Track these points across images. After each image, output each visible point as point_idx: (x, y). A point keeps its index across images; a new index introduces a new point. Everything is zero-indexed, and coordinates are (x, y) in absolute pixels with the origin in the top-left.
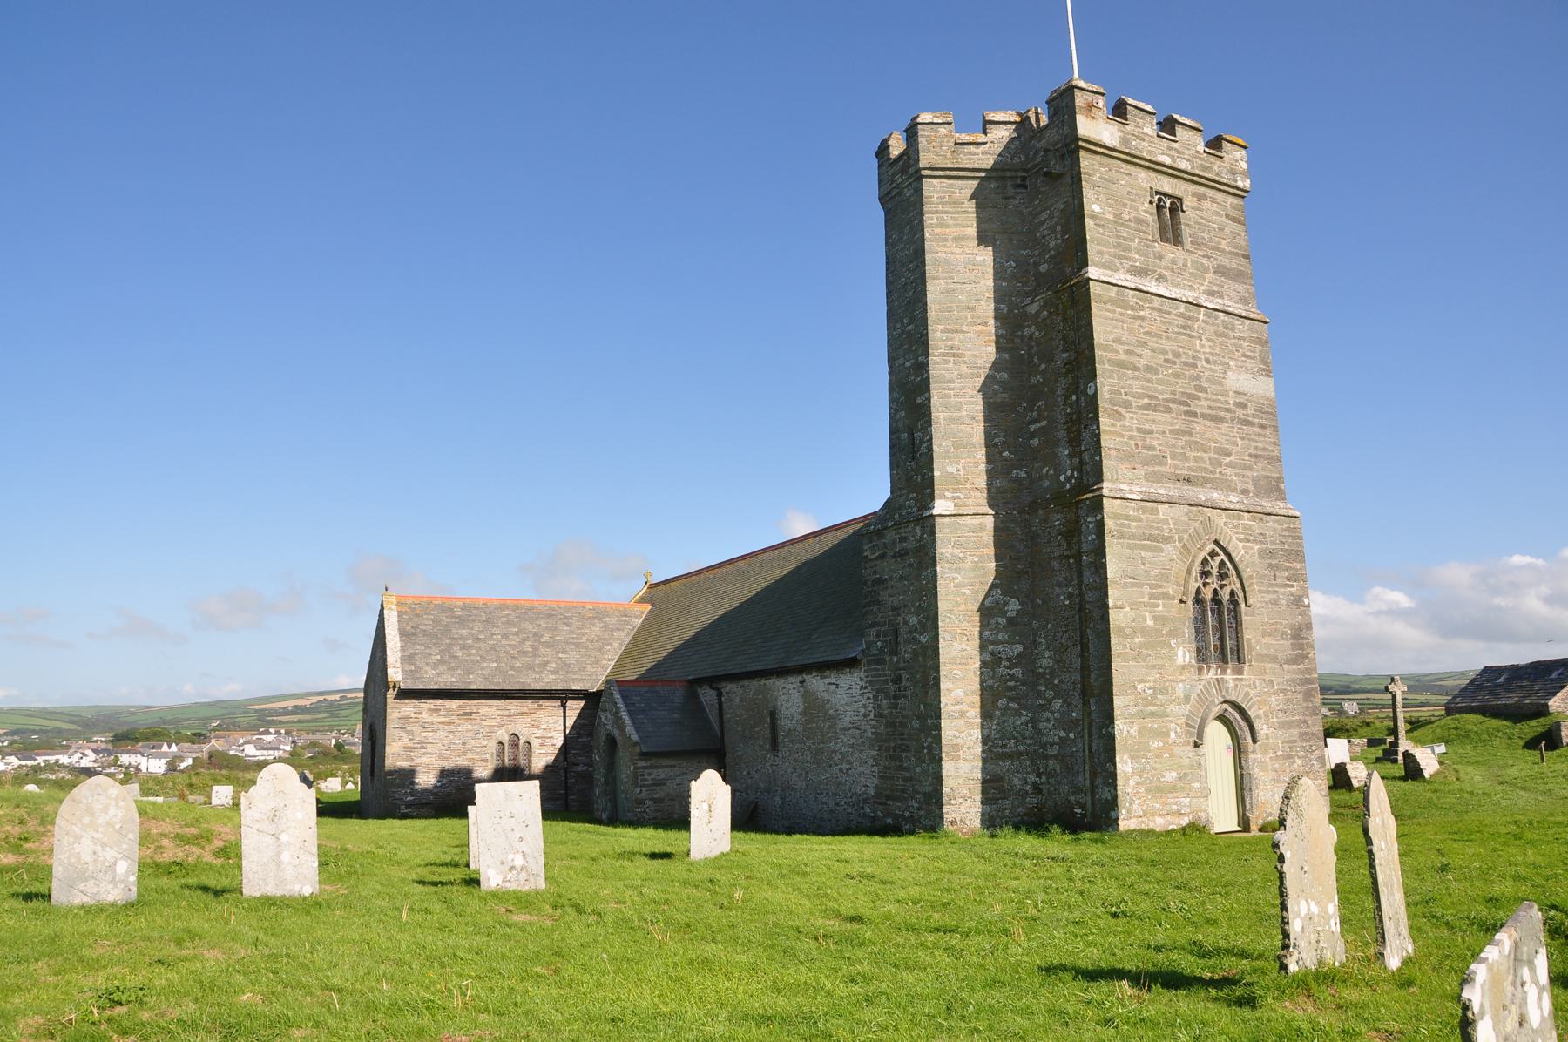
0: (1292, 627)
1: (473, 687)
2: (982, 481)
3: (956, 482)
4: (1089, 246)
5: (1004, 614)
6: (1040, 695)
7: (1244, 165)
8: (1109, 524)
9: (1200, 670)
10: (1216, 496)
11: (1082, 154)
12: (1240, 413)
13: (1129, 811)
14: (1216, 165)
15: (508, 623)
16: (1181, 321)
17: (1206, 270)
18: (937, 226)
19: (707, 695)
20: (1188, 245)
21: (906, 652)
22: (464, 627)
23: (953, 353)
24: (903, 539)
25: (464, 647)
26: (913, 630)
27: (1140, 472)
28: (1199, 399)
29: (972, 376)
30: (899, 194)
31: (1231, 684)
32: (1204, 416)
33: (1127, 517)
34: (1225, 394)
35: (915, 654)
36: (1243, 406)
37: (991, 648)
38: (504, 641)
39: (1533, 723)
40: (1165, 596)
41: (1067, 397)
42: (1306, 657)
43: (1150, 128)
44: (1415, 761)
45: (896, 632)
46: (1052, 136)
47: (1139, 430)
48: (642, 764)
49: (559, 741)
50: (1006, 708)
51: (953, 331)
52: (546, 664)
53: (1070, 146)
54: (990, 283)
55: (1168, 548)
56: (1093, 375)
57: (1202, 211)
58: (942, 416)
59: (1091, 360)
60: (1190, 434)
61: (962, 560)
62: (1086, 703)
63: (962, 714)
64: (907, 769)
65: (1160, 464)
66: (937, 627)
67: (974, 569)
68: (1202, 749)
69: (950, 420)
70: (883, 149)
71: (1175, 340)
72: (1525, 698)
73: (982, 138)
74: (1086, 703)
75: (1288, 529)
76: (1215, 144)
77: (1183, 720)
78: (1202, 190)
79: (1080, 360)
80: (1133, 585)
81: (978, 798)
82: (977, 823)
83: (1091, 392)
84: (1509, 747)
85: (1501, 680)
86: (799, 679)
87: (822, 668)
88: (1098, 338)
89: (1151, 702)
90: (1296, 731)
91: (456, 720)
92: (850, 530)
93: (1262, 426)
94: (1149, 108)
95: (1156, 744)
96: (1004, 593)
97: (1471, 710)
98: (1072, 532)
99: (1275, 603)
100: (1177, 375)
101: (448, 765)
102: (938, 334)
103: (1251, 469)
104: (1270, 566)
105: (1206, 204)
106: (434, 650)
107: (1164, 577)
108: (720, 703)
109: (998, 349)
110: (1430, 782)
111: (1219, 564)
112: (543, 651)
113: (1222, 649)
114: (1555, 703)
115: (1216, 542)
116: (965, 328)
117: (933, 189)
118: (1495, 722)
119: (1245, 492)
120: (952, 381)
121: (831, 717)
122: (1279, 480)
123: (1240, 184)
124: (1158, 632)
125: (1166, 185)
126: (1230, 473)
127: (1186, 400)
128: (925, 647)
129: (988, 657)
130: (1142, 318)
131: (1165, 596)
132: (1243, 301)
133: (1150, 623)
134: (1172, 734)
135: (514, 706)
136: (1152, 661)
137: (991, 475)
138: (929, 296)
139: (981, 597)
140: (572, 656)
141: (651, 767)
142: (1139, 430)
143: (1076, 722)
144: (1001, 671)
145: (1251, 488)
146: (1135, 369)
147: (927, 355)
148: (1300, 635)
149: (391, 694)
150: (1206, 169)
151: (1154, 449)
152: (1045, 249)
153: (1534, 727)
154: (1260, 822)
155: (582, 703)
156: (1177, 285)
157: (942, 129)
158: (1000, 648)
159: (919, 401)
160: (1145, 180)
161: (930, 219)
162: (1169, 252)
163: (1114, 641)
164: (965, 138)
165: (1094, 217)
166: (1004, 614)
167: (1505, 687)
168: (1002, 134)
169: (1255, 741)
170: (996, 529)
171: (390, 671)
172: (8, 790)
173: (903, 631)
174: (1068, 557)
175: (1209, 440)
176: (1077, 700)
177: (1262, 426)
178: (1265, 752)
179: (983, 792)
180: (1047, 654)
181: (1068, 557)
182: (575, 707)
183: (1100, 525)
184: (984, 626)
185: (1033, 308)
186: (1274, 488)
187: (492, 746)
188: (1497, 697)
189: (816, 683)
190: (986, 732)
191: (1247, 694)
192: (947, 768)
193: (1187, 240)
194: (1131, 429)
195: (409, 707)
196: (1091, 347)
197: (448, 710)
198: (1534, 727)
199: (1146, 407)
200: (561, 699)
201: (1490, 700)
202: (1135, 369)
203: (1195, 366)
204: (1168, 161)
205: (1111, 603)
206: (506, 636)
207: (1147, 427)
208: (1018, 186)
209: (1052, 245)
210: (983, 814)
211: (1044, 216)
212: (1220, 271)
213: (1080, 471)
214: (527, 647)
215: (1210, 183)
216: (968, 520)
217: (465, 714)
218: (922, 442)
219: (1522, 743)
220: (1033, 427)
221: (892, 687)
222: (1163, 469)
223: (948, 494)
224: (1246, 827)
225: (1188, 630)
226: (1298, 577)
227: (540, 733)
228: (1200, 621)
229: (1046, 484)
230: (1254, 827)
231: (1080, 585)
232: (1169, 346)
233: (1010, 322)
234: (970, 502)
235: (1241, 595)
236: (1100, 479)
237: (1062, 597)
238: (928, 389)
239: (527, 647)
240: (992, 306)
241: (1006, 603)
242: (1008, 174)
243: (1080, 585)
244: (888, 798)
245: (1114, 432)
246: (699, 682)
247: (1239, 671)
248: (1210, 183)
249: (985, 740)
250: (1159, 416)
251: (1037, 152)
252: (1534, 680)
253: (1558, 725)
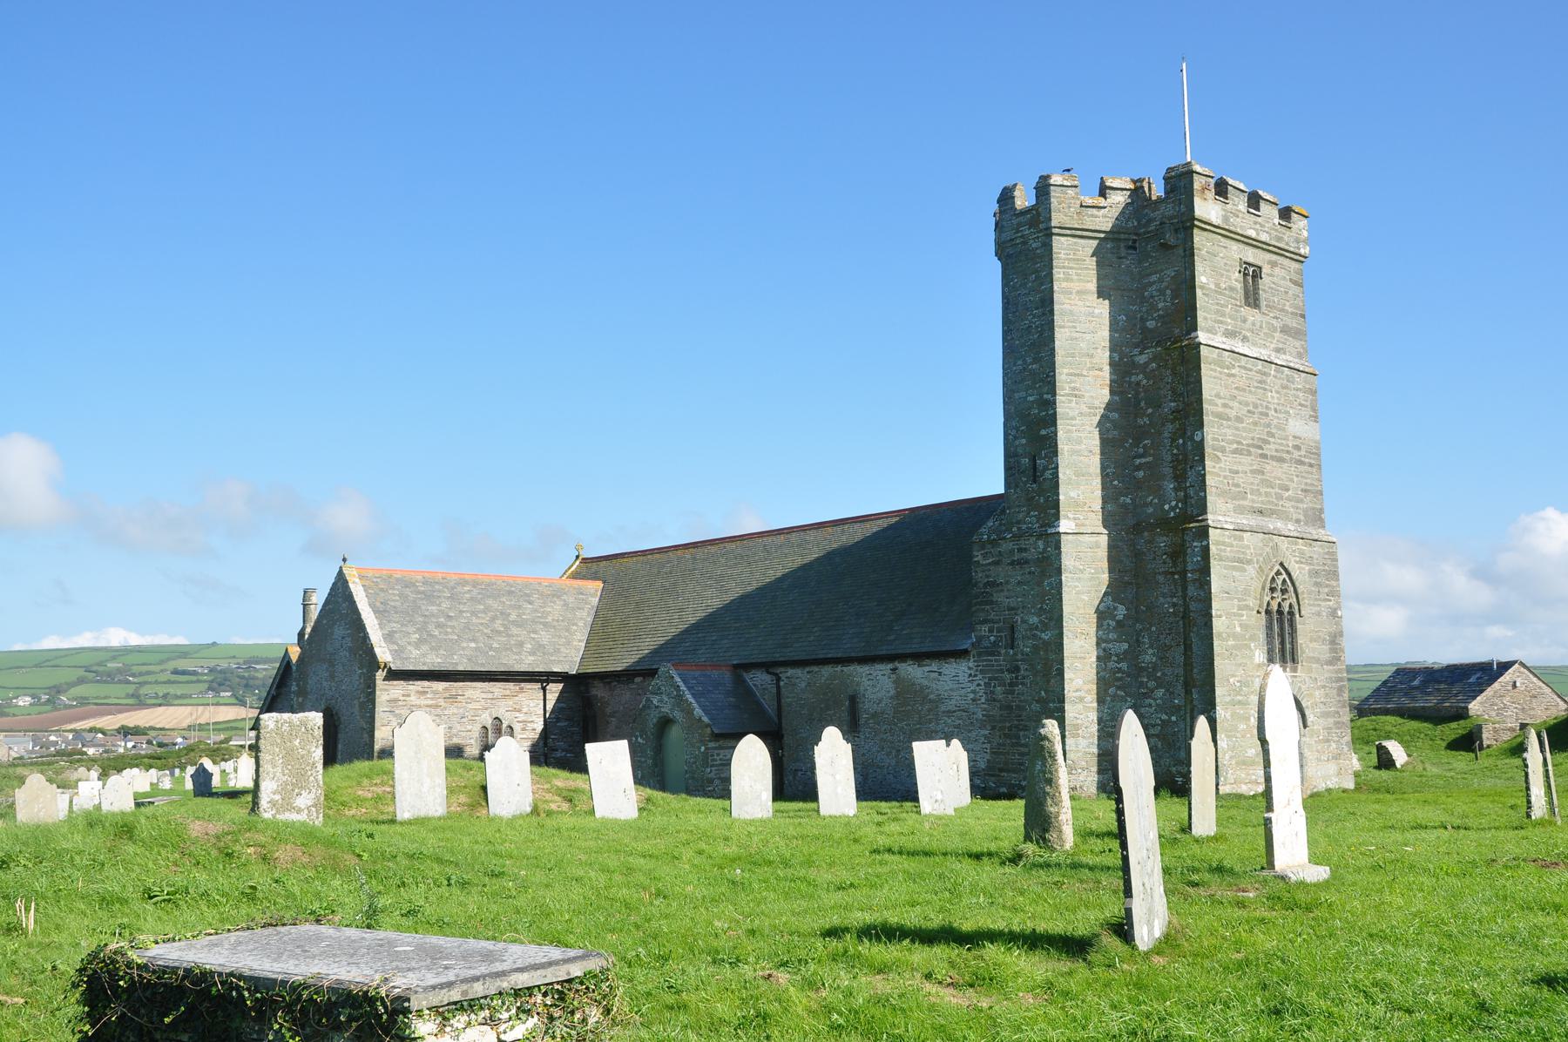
0: (1330, 634)
3: (1076, 504)
4: (1199, 313)
5: (1113, 617)
6: (1142, 685)
7: (1305, 234)
8: (1213, 549)
11: (1196, 231)
12: (1296, 454)
14: (1287, 235)
15: (472, 599)
17: (1275, 330)
19: (759, 680)
20: (1264, 309)
21: (1025, 646)
22: (433, 604)
23: (1076, 395)
24: (1021, 550)
25: (439, 626)
26: (1033, 628)
29: (1089, 414)
30: (1024, 243)
32: (1273, 458)
33: (1223, 543)
35: (1036, 648)
36: (1297, 448)
38: (474, 620)
39: (1454, 725)
40: (1247, 607)
41: (1173, 440)
43: (1242, 206)
44: (1388, 753)
45: (1012, 629)
46: (1168, 210)
48: (711, 745)
49: (540, 726)
50: (1115, 695)
52: (521, 644)
53: (1186, 223)
55: (1249, 568)
56: (1201, 425)
57: (1276, 276)
59: (1199, 412)
61: (1082, 571)
62: (1188, 692)
63: (1081, 699)
64: (1025, 745)
66: (1061, 627)
67: (1091, 579)
69: (1073, 452)
70: (1006, 197)
72: (1443, 701)
73: (1102, 202)
74: (1188, 692)
76: (1286, 214)
78: (1275, 257)
79: (1190, 411)
81: (1095, 769)
82: (1093, 790)
83: (1197, 439)
84: (1432, 748)
85: (1416, 683)
86: (890, 666)
87: (919, 657)
88: (1206, 394)
89: (1239, 694)
90: (1331, 720)
91: (442, 702)
92: (884, 523)
93: (1311, 465)
94: (1242, 187)
95: (1242, 726)
97: (1387, 712)
98: (1178, 553)
99: (1319, 614)
100: (1255, 424)
103: (1301, 501)
104: (1317, 584)
105: (1277, 270)
106: (411, 629)
107: (1246, 592)
108: (778, 687)
109: (1111, 392)
110: (1401, 771)
111: (1282, 582)
112: (515, 630)
113: (1283, 650)
114: (1475, 707)
115: (1281, 564)
117: (1061, 245)
118: (1415, 724)
119: (1298, 521)
120: (1073, 418)
121: (931, 701)
122: (1321, 511)
123: (1302, 251)
125: (1252, 255)
128: (1046, 644)
131: (1247, 607)
132: (1300, 355)
133: (1238, 629)
135: (497, 688)
137: (1105, 500)
138: (1057, 343)
140: (545, 637)
141: (721, 748)
143: (1178, 708)
144: (1111, 665)
146: (1229, 419)
147: (1054, 394)
148: (1335, 640)
149: (380, 675)
150: (1279, 239)
152: (1154, 308)
153: (1455, 729)
155: (560, 686)
156: (1254, 344)
157: (1071, 192)
159: (1043, 432)
160: (1237, 252)
161: (1058, 274)
162: (1251, 314)
163: (1216, 643)
164: (1089, 201)
165: (1202, 288)
166: (1113, 617)
167: (1422, 688)
168: (1119, 200)
170: (1110, 547)
171: (377, 651)
172: (3, 771)
173: (1021, 630)
174: (1173, 574)
176: (1179, 689)
177: (1311, 465)
179: (1099, 764)
180: (1150, 651)
181: (1173, 574)
182: (555, 689)
183: (1206, 551)
184: (1099, 626)
185: (1142, 359)
186: (1317, 518)
187: (477, 728)
188: (1413, 699)
189: (910, 670)
193: (1263, 303)
195: (398, 689)
196: (1200, 401)
197: (435, 693)
198: (1455, 729)
199: (1235, 452)
200: (541, 682)
201: (1406, 702)
202: (1229, 419)
204: (1252, 234)
206: (473, 613)
209: (1161, 305)
211: (1154, 278)
212: (1285, 330)
213: (1185, 503)
214: (498, 625)
215: (1280, 252)
217: (452, 697)
218: (1046, 469)
219: (1444, 744)
220: (1138, 461)
221: (1007, 676)
222: (1245, 503)
225: (1262, 635)
226: (1334, 593)
227: (522, 717)
228: (1269, 627)
229: (1151, 510)
231: (1184, 597)
232: (1251, 399)
233: (1122, 369)
236: (1204, 511)
237: (1167, 605)
238: (1054, 424)
239: (498, 625)
243: (1184, 597)
244: (1001, 770)
245: (1217, 471)
246: (742, 667)
247: (1295, 670)
248: (1280, 252)
249: (1100, 721)
250: (1245, 459)
251: (1150, 221)
252: (1452, 684)
253: (1480, 727)
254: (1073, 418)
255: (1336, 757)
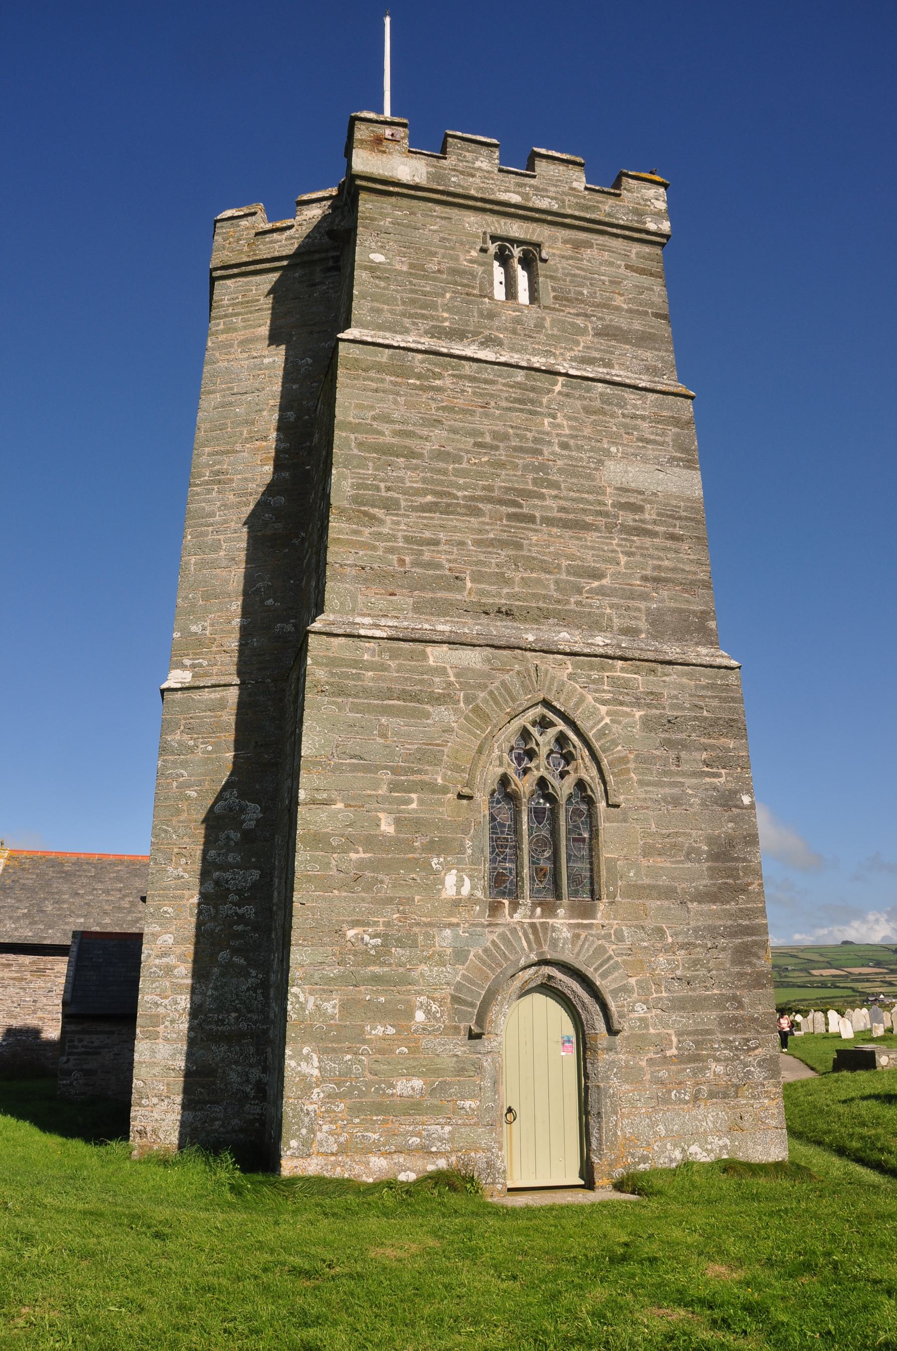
1: (47, 942)
2: (233, 643)
7: (662, 205)
9: (494, 909)
10: (564, 637)
12: (628, 518)
13: (306, 1143)
16: (516, 393)
18: (223, 332)
23: (220, 479)
27: (404, 600)
28: (542, 497)
31: (566, 934)
32: (549, 521)
34: (600, 491)
37: (216, 874)
38: (104, 897)
42: (744, 890)
47: (407, 539)
51: (223, 453)
54: (277, 387)
55: (442, 714)
58: (193, 560)
60: (519, 546)
61: (191, 750)
63: (169, 970)
65: (449, 588)
67: (205, 762)
68: (486, 1044)
71: (499, 418)
75: (711, 687)
77: (450, 990)
78: (583, 236)
80: (354, 768)
81: (179, 1099)
91: (28, 976)
93: (673, 537)
96: (241, 796)
99: (676, 801)
100: (501, 465)
101: (16, 1023)
102: (204, 459)
103: (644, 597)
104: (668, 744)
109: (278, 467)
116: (238, 447)
119: (630, 632)
123: (652, 226)
124: (406, 845)
125: (515, 229)
126: (605, 607)
127: (511, 498)
129: (210, 887)
130: (439, 389)
133: (387, 827)
134: (420, 1016)
136: (386, 889)
137: (246, 632)
139: (210, 802)
142: (407, 539)
144: (226, 909)
145: (643, 625)
150: (587, 208)
151: (439, 566)
154: (619, 1172)
158: (228, 875)
169: (612, 1031)
170: (242, 705)
175: (557, 555)
177: (673, 537)
178: (638, 1050)
179: (187, 1091)
190: (198, 999)
191: (601, 950)
192: (142, 1049)
194: (394, 538)
197: (21, 965)
203: (541, 453)
204: (515, 199)
205: (302, 795)
206: (107, 892)
207: (427, 534)
208: (329, 269)
210: (183, 1124)
216: (206, 695)
217: (38, 970)
223: (187, 662)
224: (589, 1182)
230: (600, 1181)
234: (215, 670)
235: (599, 789)
240: (276, 416)
241: (243, 810)
242: (316, 256)
247: (588, 912)
249: (195, 1012)
250: (453, 521)
254: (212, 514)
255: (722, 1093)
